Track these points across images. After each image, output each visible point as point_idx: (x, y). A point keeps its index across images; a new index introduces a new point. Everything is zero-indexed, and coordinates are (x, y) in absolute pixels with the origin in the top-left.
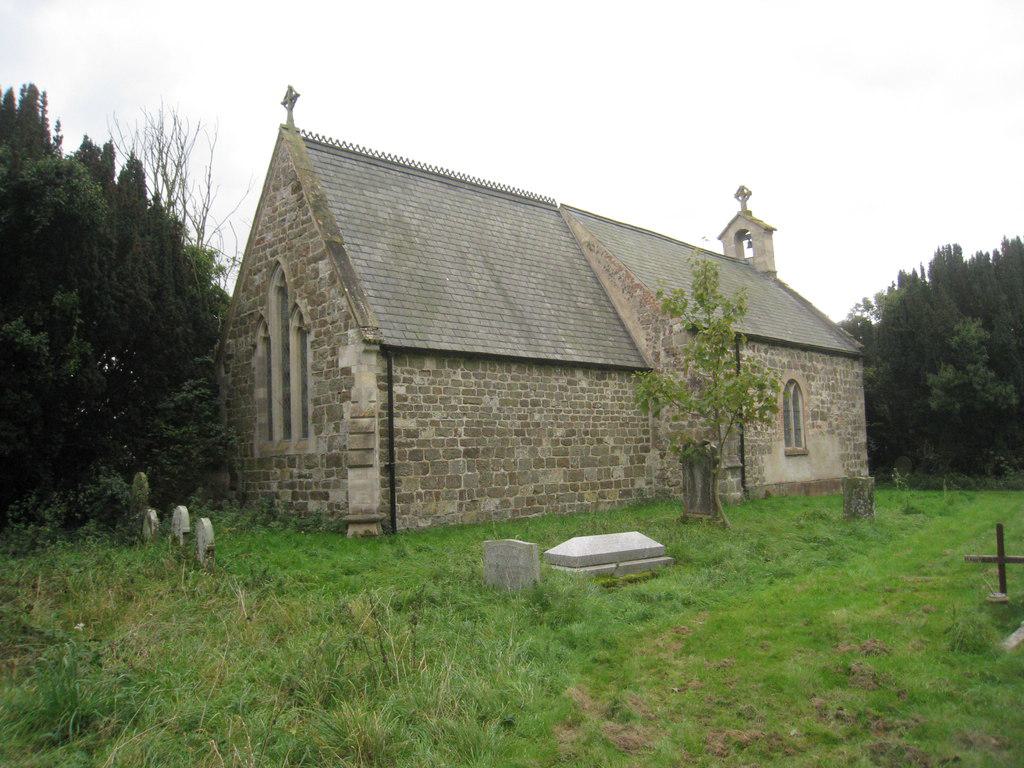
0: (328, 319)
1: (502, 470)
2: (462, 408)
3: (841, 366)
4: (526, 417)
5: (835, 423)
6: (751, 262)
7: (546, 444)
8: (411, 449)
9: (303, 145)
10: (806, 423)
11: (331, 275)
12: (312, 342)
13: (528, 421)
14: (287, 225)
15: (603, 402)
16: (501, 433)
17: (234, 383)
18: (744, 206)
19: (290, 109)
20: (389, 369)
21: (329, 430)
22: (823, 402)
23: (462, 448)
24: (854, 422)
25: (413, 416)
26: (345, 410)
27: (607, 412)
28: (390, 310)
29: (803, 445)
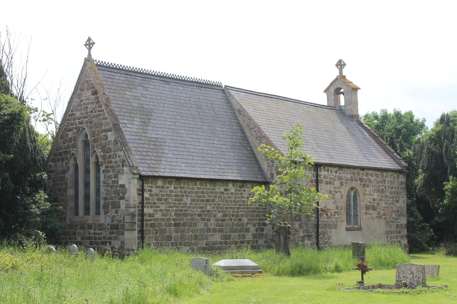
0: (113, 160)
1: (191, 233)
2: (174, 203)
3: (389, 178)
4: (203, 208)
5: (382, 212)
6: (343, 108)
7: (213, 221)
8: (151, 222)
9: (96, 68)
10: (362, 211)
11: (115, 140)
12: (103, 170)
13: (204, 209)
14: (89, 110)
15: (242, 199)
16: (191, 215)
17: (54, 185)
18: (341, 72)
19: (90, 49)
20: (143, 186)
21: (112, 212)
22: (374, 200)
23: (173, 222)
24: (398, 211)
25: (152, 207)
26: (121, 204)
27: (244, 205)
28: (142, 157)
29: (359, 225)
